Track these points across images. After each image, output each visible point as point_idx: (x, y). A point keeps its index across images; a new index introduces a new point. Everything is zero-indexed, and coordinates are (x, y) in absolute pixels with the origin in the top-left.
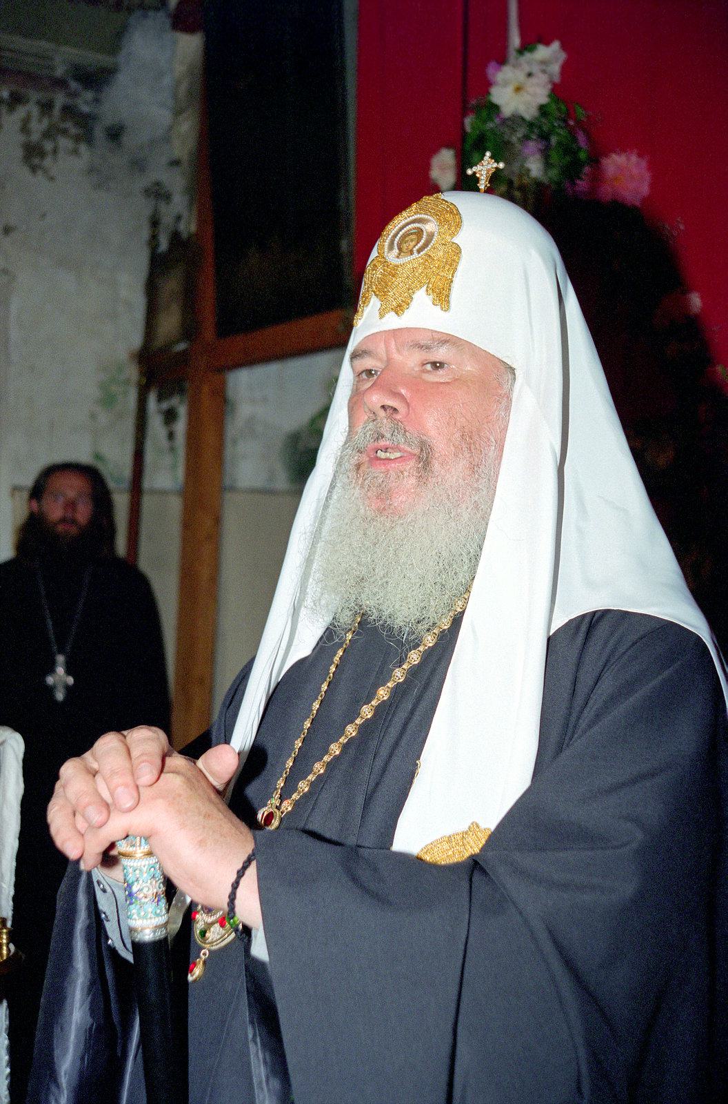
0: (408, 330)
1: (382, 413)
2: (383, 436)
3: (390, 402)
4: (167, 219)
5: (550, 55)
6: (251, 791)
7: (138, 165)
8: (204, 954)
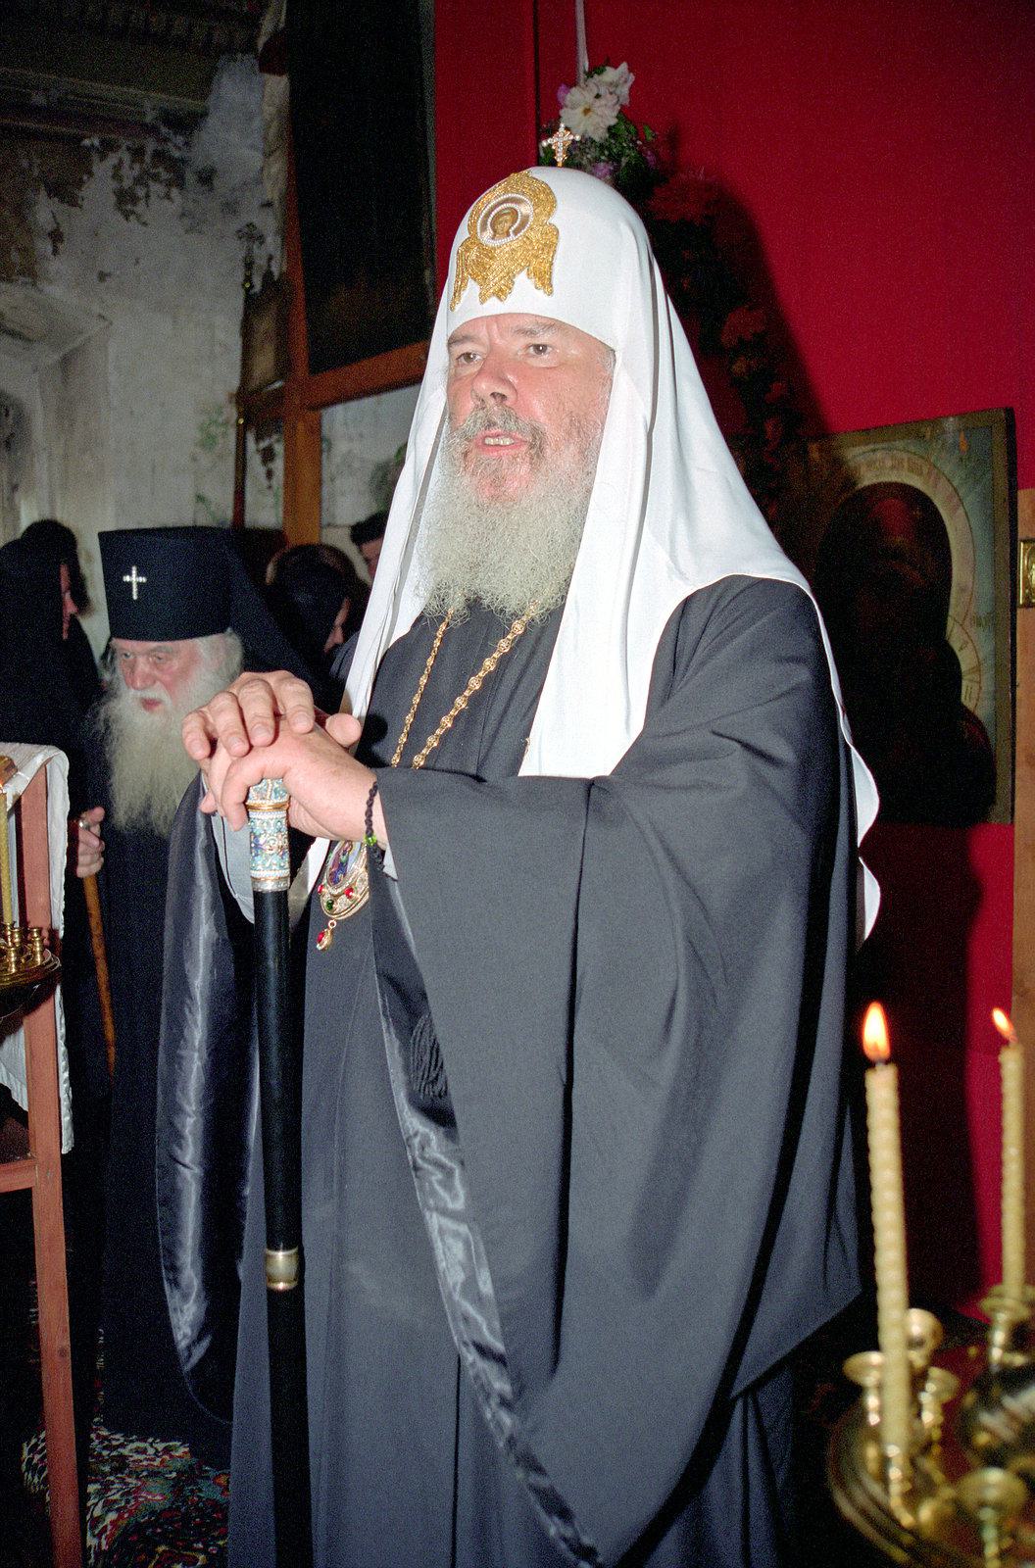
0: (511, 315)
1: (491, 401)
2: (495, 424)
3: (500, 390)
4: (261, 262)
5: (618, 76)
6: (377, 749)
7: (230, 208)
8: (332, 924)
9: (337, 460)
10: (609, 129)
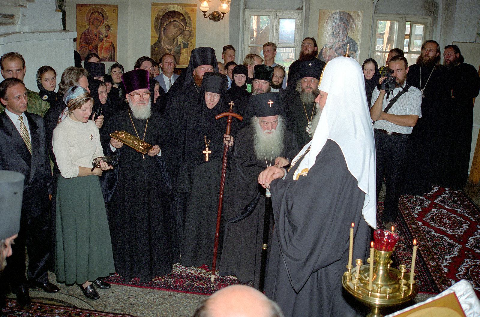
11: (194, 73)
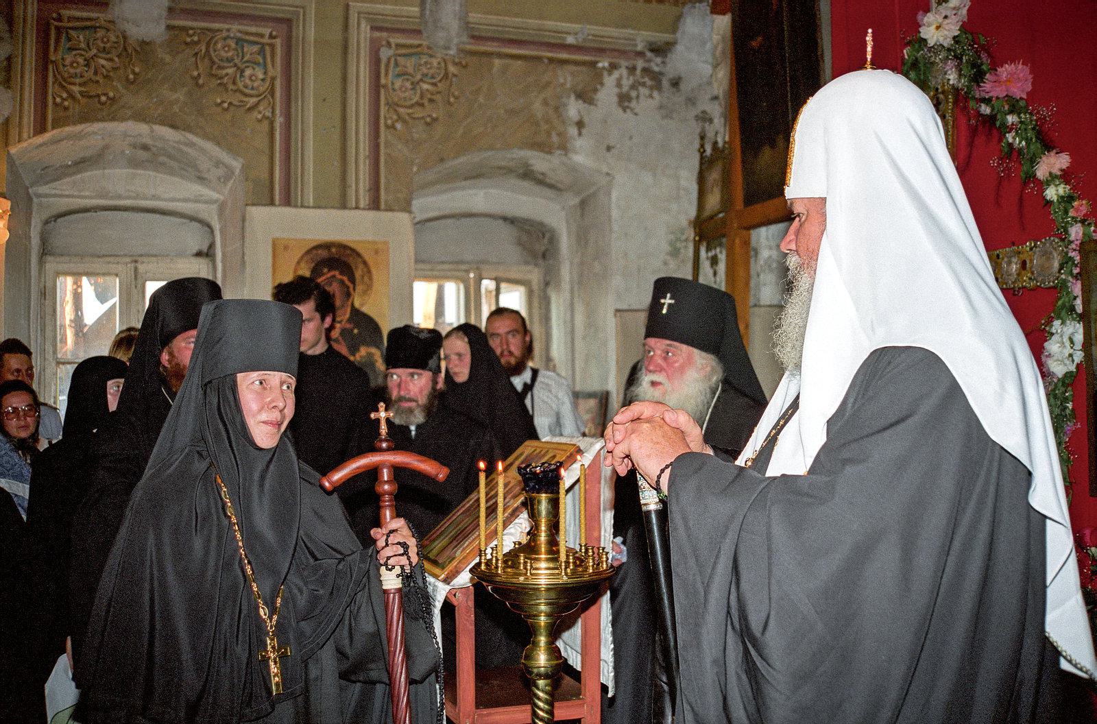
4: (710, 135)
7: (691, 101)
9: (762, 262)
10: (954, 38)
11: (165, 357)
